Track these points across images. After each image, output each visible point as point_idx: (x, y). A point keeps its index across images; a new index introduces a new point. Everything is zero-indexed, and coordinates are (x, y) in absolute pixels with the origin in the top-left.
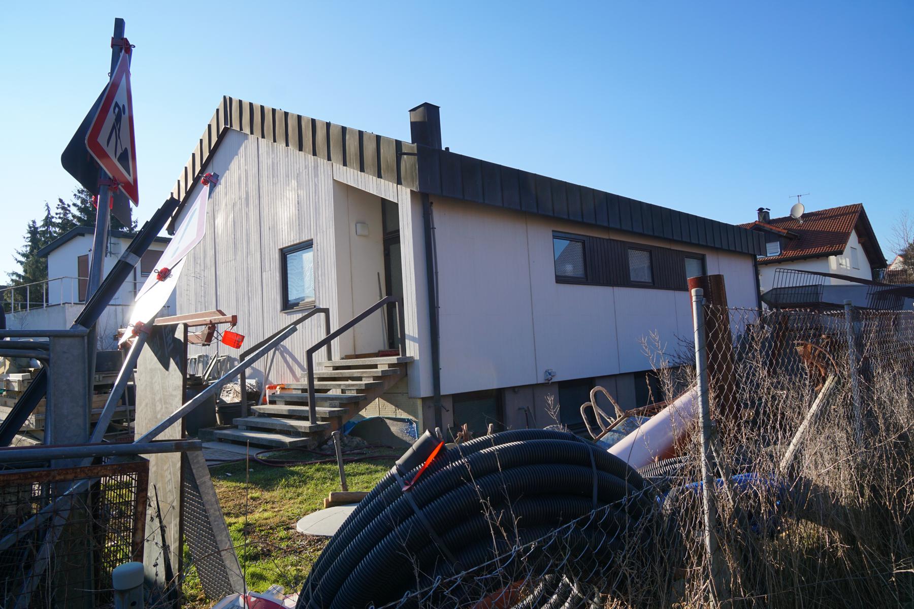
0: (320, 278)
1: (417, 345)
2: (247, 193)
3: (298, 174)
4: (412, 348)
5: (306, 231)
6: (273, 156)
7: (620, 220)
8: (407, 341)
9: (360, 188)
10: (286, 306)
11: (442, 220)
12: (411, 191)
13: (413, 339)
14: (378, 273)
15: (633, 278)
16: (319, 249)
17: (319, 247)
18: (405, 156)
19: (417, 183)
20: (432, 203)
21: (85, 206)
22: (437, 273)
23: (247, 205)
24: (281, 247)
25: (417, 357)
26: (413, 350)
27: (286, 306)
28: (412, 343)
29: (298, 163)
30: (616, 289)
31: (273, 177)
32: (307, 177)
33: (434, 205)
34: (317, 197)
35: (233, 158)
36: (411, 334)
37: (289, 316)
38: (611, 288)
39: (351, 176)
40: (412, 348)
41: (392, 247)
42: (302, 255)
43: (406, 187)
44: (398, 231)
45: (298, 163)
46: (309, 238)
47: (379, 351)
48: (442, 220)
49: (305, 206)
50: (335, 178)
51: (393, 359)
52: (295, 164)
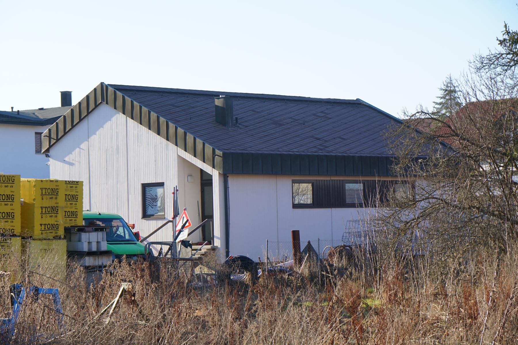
0: (168, 204)
1: (220, 241)
2: (118, 146)
3: (155, 145)
4: (217, 242)
5: (160, 177)
6: (138, 130)
7: (336, 171)
8: (215, 239)
9: (193, 163)
10: (145, 216)
11: (234, 182)
12: (219, 173)
13: (218, 238)
14: (198, 201)
15: (348, 201)
16: (168, 189)
17: (168, 187)
18: (217, 156)
19: (222, 170)
20: (228, 176)
21: (259, 277)
22: (229, 208)
23: (118, 152)
24: (143, 183)
25: (219, 246)
26: (218, 243)
27: (145, 216)
28: (217, 240)
29: (155, 139)
30: (333, 209)
31: (138, 142)
32: (161, 149)
33: (229, 177)
34: (167, 161)
35: (107, 122)
36: (217, 236)
37: (148, 222)
38: (330, 209)
39: (188, 157)
40: (217, 242)
41: (206, 188)
42: (156, 190)
43: (217, 170)
44: (212, 180)
45: (155, 139)
46: (162, 182)
47: (198, 243)
48: (232, 181)
49: (160, 164)
50: (178, 154)
51: (209, 247)
52: (153, 139)
